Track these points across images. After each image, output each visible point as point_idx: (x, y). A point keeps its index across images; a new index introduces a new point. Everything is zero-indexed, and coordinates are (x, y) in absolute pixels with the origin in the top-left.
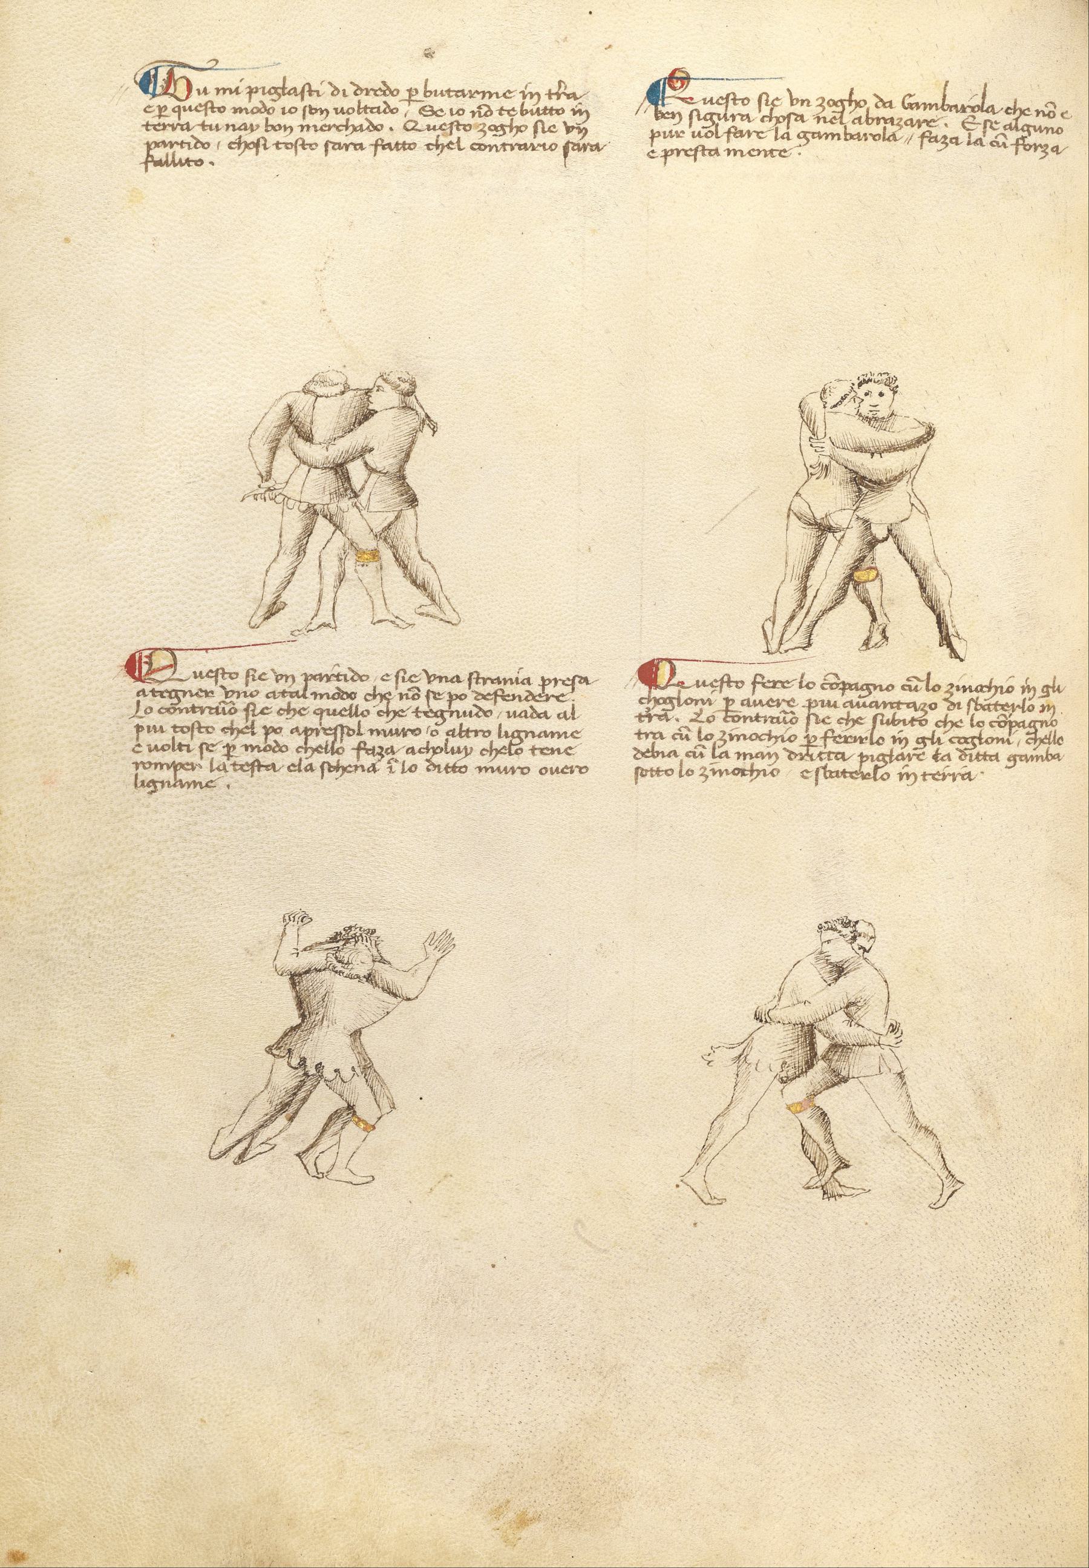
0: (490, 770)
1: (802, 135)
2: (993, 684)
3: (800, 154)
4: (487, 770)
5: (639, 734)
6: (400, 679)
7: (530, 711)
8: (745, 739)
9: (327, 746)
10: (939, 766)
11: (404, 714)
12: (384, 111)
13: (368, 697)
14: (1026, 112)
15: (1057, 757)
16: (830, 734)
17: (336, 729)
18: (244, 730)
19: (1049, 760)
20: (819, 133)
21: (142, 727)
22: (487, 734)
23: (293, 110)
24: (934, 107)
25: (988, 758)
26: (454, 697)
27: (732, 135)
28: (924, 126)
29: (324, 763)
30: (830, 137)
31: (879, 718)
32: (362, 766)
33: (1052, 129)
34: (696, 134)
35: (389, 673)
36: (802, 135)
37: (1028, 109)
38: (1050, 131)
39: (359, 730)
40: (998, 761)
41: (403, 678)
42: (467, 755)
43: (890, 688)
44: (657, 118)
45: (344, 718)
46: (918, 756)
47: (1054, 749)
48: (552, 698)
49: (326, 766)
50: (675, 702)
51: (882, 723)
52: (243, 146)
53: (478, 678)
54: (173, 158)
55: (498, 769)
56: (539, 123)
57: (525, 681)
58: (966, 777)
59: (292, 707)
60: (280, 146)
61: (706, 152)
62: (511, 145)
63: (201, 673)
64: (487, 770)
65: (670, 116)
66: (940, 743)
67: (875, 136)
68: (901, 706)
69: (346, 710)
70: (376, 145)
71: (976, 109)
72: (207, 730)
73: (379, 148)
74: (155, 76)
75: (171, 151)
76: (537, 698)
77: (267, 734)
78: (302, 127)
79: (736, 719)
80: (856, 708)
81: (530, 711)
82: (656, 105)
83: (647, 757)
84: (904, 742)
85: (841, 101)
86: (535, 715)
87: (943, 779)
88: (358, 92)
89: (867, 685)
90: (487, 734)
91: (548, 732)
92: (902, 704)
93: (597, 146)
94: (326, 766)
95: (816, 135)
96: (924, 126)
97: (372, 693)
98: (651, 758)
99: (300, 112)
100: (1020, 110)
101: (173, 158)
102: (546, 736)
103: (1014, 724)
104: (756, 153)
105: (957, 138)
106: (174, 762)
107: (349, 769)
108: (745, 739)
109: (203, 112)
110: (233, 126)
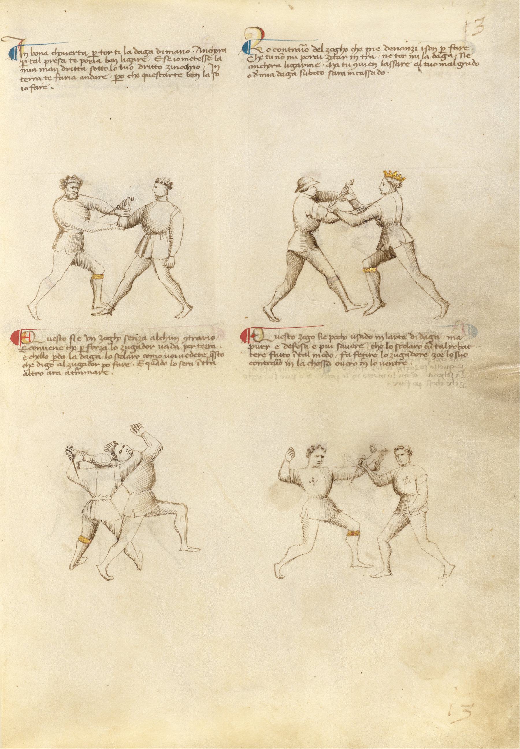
2: (357, 47)
6: (302, 74)
9: (393, 67)
12: (473, 64)
15: (416, 48)
18: (111, 61)
23: (307, 50)
24: (444, 65)
25: (103, 69)
26: (303, 58)
31: (303, 71)
34: (161, 347)
35: (63, 346)
37: (362, 48)
38: (171, 53)
40: (221, 60)
41: (304, 73)
44: (40, 77)
45: (319, 52)
48: (274, 66)
53: (218, 354)
56: (428, 47)
57: (207, 75)
58: (273, 364)
59: (357, 47)
60: (196, 59)
61: (62, 339)
68: (196, 59)
69: (201, 58)
70: (451, 47)
71: (38, 79)
74: (249, 330)
76: (391, 49)
77: (82, 63)
79: (36, 54)
80: (260, 68)
83: (319, 51)
85: (337, 49)
91: (404, 47)
92: (319, 72)
97: (354, 48)
98: (334, 48)
99: (178, 364)
105: (75, 77)
106: (114, 59)
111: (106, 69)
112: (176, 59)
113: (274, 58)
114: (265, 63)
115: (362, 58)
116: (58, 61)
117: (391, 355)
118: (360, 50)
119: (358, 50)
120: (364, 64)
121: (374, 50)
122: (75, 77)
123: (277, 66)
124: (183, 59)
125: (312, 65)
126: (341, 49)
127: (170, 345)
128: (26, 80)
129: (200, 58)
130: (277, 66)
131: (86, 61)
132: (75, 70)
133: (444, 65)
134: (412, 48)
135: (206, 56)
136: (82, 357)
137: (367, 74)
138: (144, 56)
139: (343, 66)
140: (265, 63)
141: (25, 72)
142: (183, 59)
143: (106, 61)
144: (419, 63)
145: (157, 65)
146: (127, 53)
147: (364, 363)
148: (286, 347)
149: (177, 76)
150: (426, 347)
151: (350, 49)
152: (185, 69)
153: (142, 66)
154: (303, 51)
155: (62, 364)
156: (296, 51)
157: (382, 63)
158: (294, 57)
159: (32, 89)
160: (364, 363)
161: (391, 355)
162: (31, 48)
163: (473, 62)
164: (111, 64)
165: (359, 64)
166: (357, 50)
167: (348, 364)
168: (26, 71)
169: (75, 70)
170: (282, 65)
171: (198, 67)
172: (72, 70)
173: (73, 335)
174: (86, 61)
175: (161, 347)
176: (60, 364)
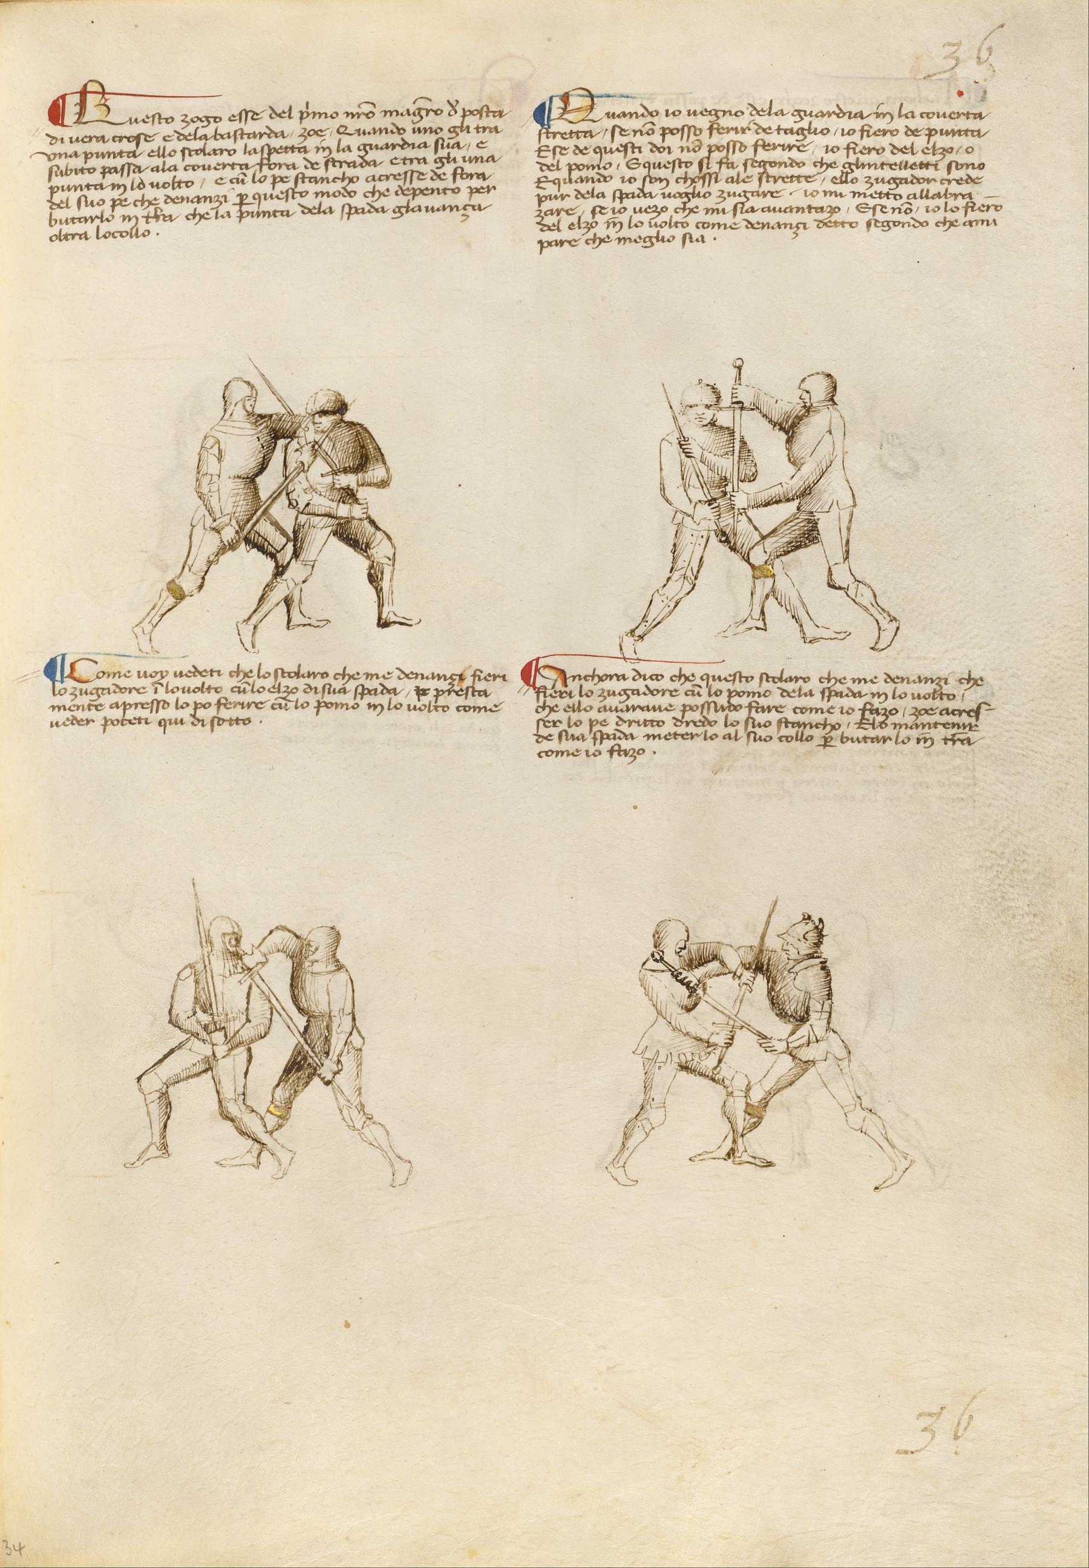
1: (452, 130)
2: (596, 673)
4: (59, 708)
5: (53, 707)
7: (380, 688)
8: (65, 709)
11: (806, 149)
13: (674, 678)
17: (152, 702)
19: (67, 240)
21: (167, 672)
22: (247, 722)
28: (801, 682)
29: (762, 674)
30: (318, 116)
36: (397, 210)
46: (96, 707)
50: (445, 161)
51: (86, 206)
62: (774, 177)
64: (59, 708)
67: (368, 114)
72: (787, 739)
75: (408, 185)
78: (176, 169)
82: (53, 681)
83: (61, 208)
86: (385, 691)
93: (980, 115)
95: (312, 180)
96: (801, 682)
98: (672, 127)
100: (549, 707)
104: (956, 116)
108: (65, 709)
110: (204, 169)
112: (846, 132)
113: (917, 113)
115: (779, 133)
116: (732, 678)
117: (73, 690)
118: (356, 676)
121: (725, 228)
124: (825, 192)
126: (593, 677)
127: (112, 688)
128: (547, 724)
131: (655, 692)
135: (129, 164)
138: (620, 702)
142: (825, 192)
148: (385, 691)
149: (782, 132)
151: (331, 675)
154: (655, 710)
155: (733, 735)
158: (991, 221)
159: (848, 152)
161: (73, 690)
164: (895, 688)
166: (198, 217)
167: (382, 178)
169: (936, 728)
174: (675, 131)
175: (142, 674)
176: (729, 735)
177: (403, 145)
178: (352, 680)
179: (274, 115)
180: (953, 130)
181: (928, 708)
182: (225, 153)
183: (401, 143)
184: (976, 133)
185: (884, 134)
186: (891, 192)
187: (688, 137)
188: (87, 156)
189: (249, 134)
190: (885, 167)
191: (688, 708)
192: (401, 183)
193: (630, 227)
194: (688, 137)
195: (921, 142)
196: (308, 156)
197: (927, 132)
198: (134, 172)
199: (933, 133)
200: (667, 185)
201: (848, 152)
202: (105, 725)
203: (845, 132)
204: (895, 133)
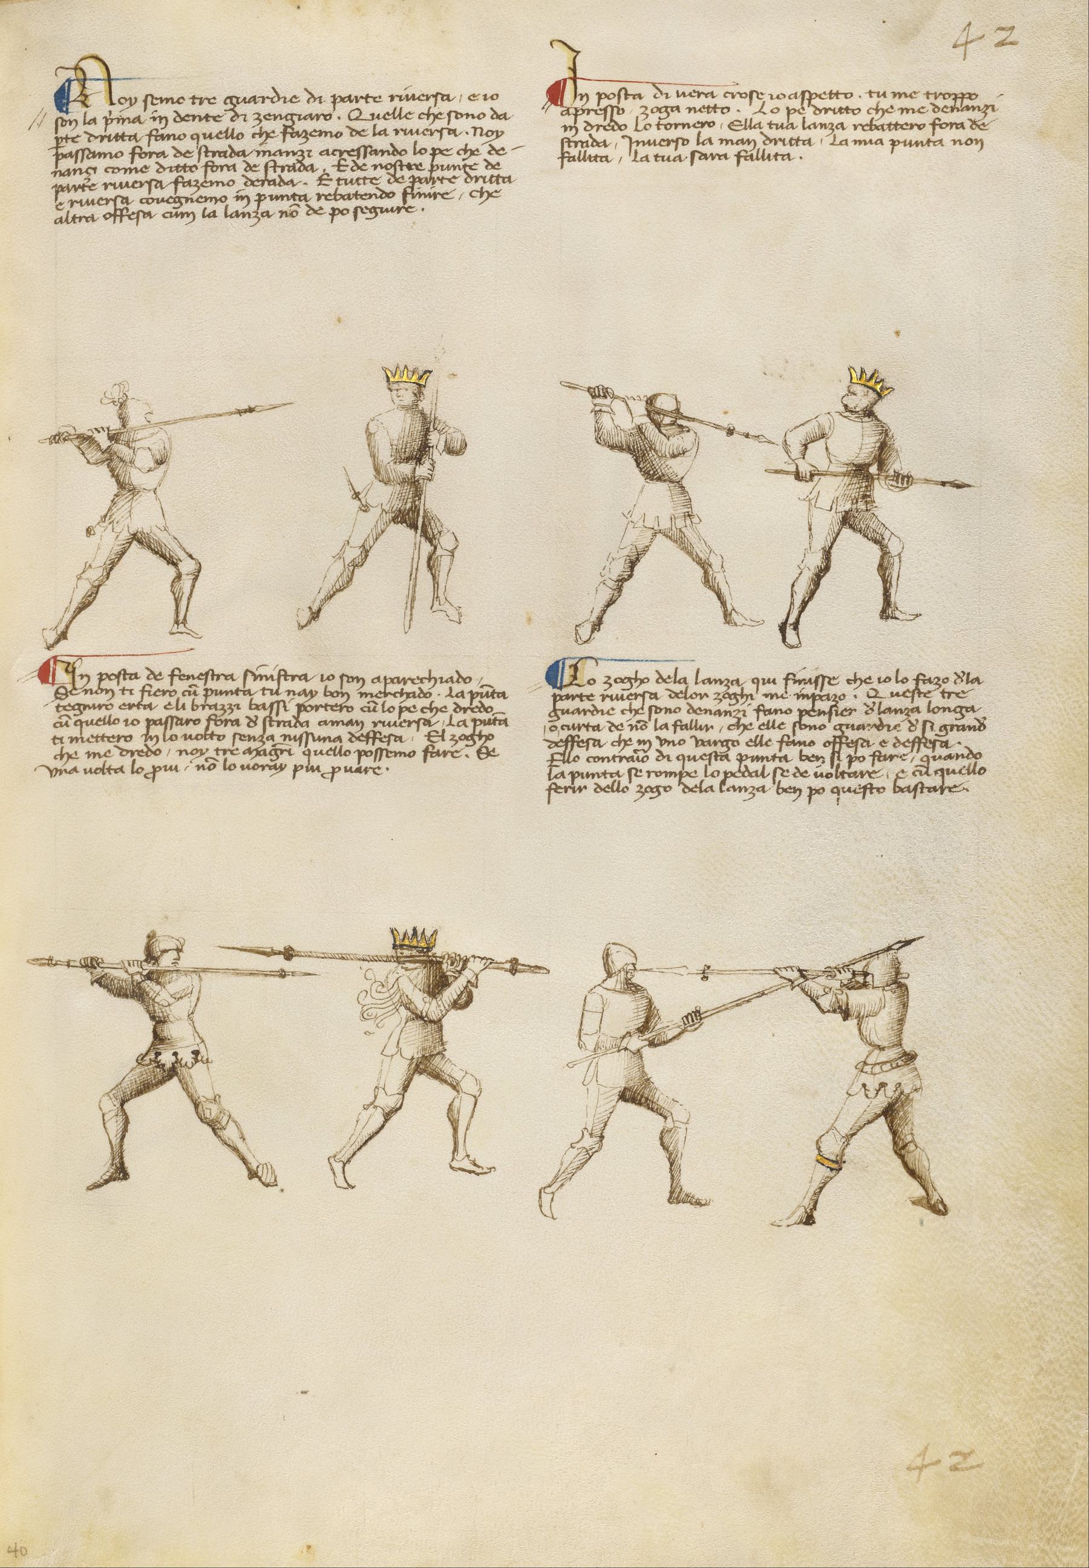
0: (134, 171)
3: (282, 1190)
10: (359, 174)
14: (272, 135)
16: (154, 133)
20: (398, 678)
22: (128, 739)
27: (678, 728)
32: (136, 168)
33: (331, 132)
39: (874, 760)
42: (131, 105)
43: (482, 116)
47: (977, 134)
48: (320, 709)
49: (654, 708)
52: (486, 195)
54: (763, 153)
55: (411, 131)
63: (389, 722)
65: (318, 133)
66: (196, 695)
73: (153, 138)
81: (278, 181)
84: (155, 739)
87: (107, 204)
88: (660, 758)
89: (292, 115)
90: (128, 739)
93: (232, 676)
94: (654, 708)
101: (763, 153)
102: (735, 790)
103: (603, 96)
105: (842, 124)
107: (256, 183)
109: (910, 699)
111: (725, 111)
114: (466, 145)
115: (123, 694)
118: (272, 135)
119: (745, 727)
120: (308, 691)
122: (842, 124)
123: (158, 155)
125: (172, 99)
129: (353, 150)
130: (158, 155)
132: (117, 140)
133: (97, 756)
134: (304, 135)
136: (691, 711)
137: (169, 725)
139: (656, 160)
140: (466, 145)
141: (130, 172)
143: (894, 789)
144: (876, 761)
145: (126, 134)
146: (809, 127)
147: (242, 198)
150: (58, 725)
152: (605, 95)
153: (461, 709)
156: (87, 221)
157: (698, 140)
159: (934, 129)
160: (242, 198)
162: (172, 685)
163: (968, 752)
165: (689, 756)
166: (486, 195)
168: (134, 171)
169: (117, 140)
170: (345, 737)
171: (982, 771)
172: (81, 205)
173: (624, 88)
177: (879, 726)
178: (439, 713)
179: (660, 681)
180: (757, 756)
181: (418, 163)
182: (267, 101)
183: (592, 709)
184: (133, 677)
185: (912, 128)
186: (662, 122)
187: (580, 154)
188: (360, 754)
189: (804, 141)
190: (840, 96)
191: (437, 152)
192: (355, 158)
193: (415, 154)
194: (580, 154)
195: (426, 160)
196: (247, 159)
197: (257, 198)
198: (156, 187)
199: (263, 198)
200: (194, 219)
201: (934, 129)
202: (333, 215)
203: (325, 678)
204: (328, 118)
